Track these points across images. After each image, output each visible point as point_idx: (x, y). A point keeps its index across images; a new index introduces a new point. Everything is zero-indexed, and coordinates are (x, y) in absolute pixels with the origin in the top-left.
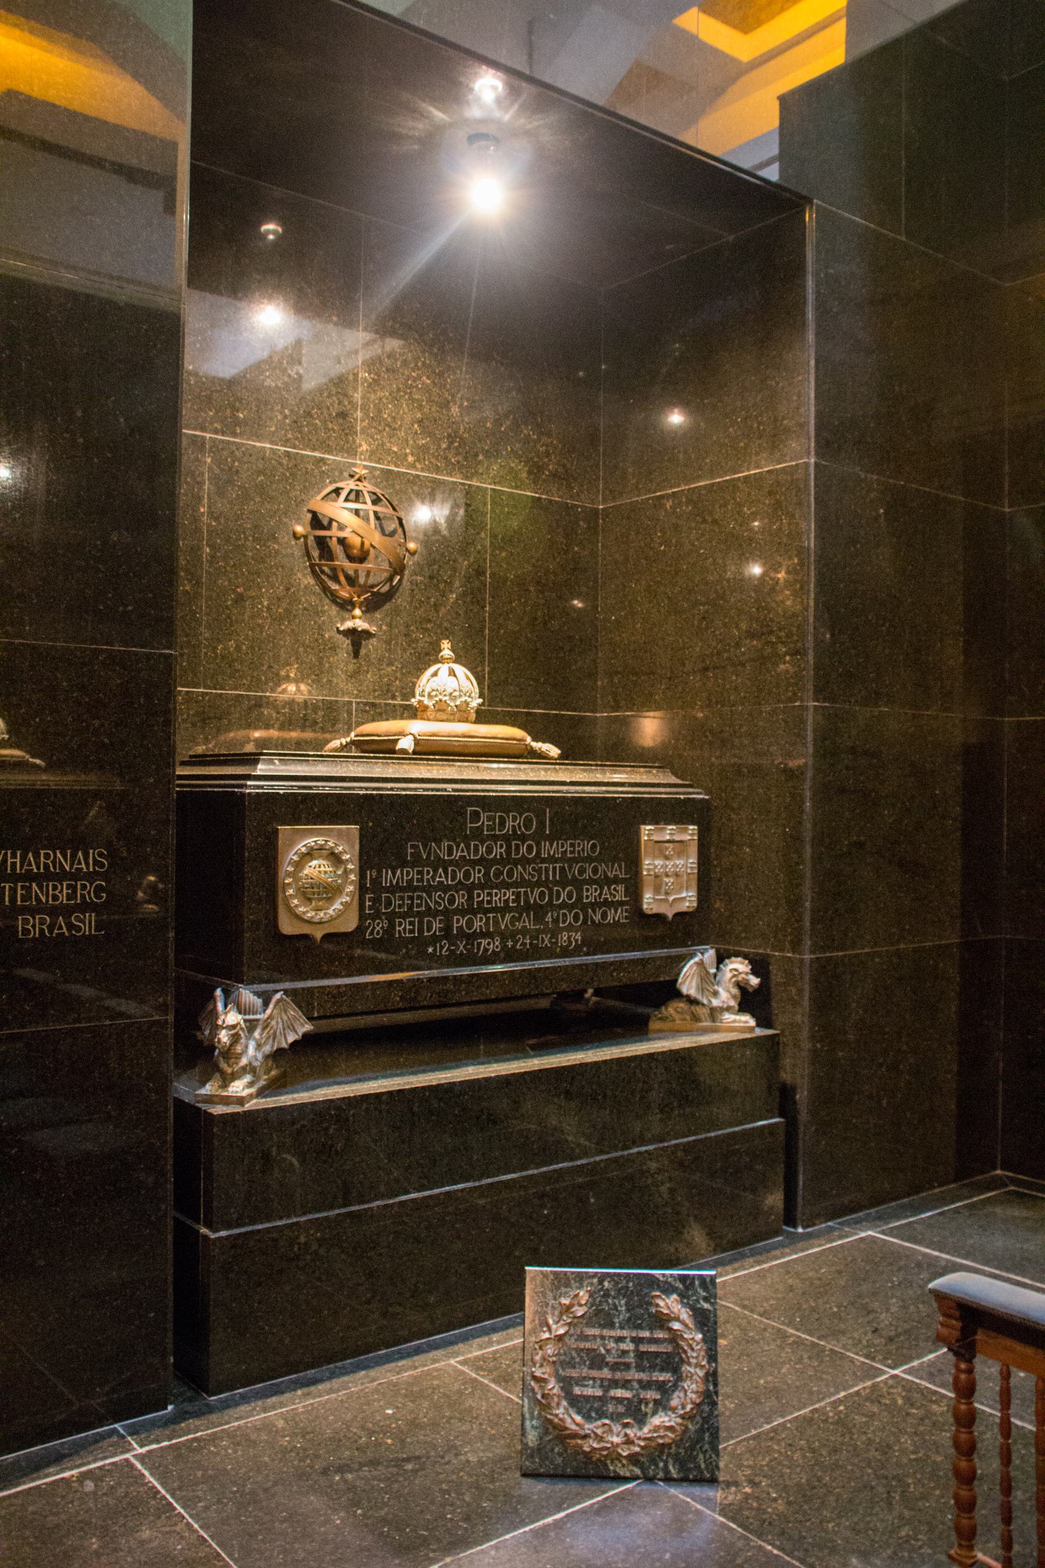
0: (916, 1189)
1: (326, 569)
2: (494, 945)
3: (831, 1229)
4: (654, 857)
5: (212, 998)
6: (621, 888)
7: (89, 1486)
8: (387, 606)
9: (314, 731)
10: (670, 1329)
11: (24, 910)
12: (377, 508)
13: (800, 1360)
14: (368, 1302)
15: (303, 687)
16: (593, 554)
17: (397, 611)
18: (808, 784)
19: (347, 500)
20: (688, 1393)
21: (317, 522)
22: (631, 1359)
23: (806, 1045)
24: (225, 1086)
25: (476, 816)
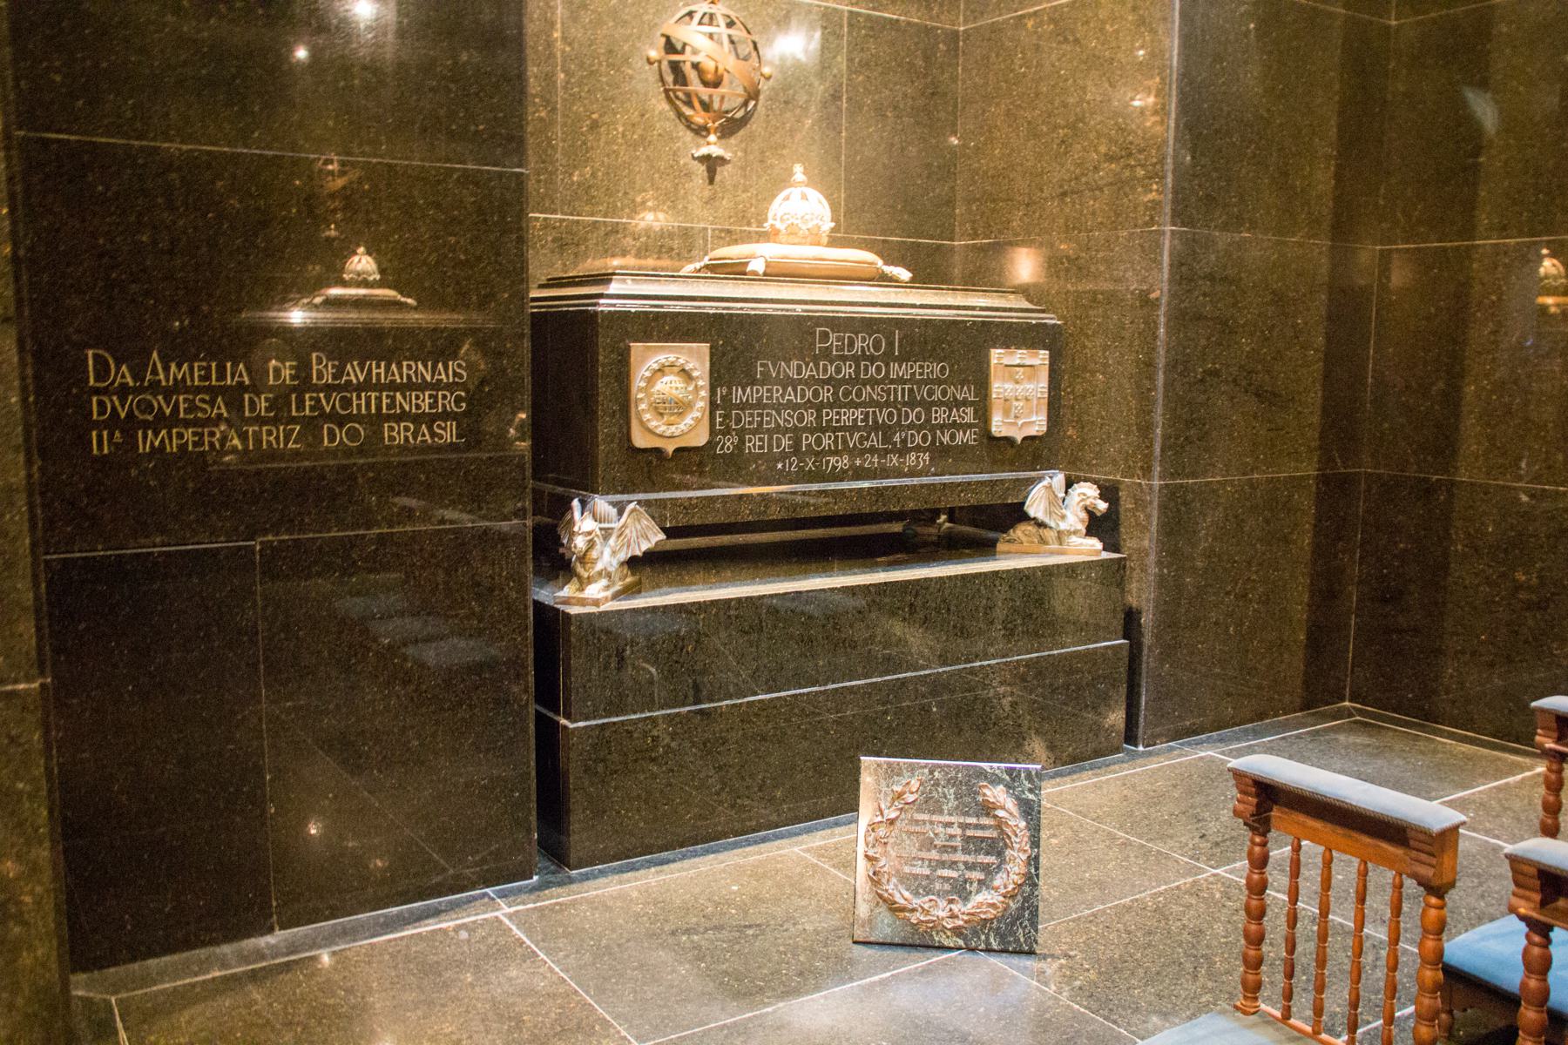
0: (1261, 716)
1: (680, 94)
2: (843, 462)
3: (1172, 749)
4: (1004, 381)
5: (570, 508)
6: (970, 410)
7: (464, 935)
8: (742, 132)
9: (671, 258)
10: (995, 817)
11: (388, 418)
12: (731, 31)
13: (1127, 858)
14: (718, 794)
15: (661, 216)
16: (954, 79)
17: (752, 137)
18: (1163, 310)
19: (700, 23)
20: (1012, 874)
21: (670, 47)
22: (958, 842)
23: (1153, 570)
24: (581, 590)
25: (825, 336)
